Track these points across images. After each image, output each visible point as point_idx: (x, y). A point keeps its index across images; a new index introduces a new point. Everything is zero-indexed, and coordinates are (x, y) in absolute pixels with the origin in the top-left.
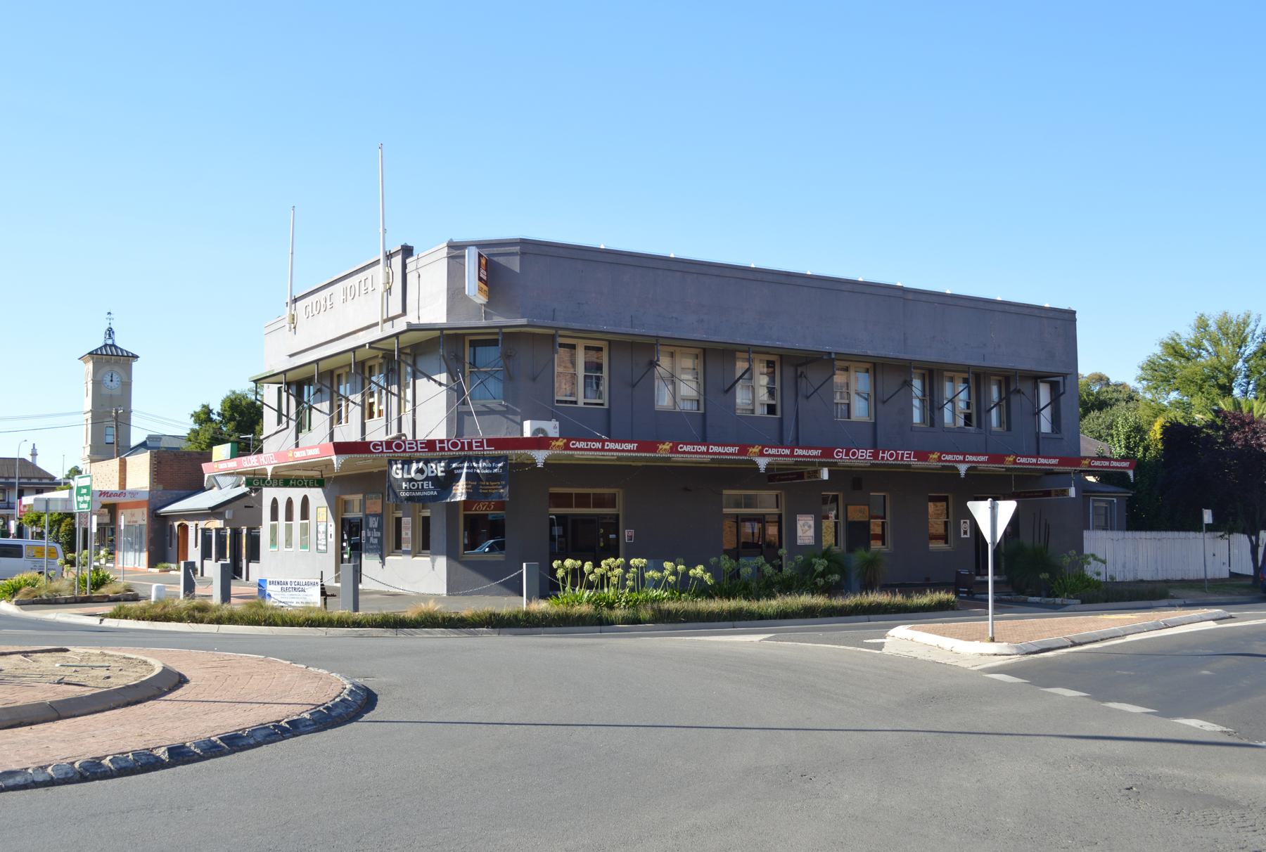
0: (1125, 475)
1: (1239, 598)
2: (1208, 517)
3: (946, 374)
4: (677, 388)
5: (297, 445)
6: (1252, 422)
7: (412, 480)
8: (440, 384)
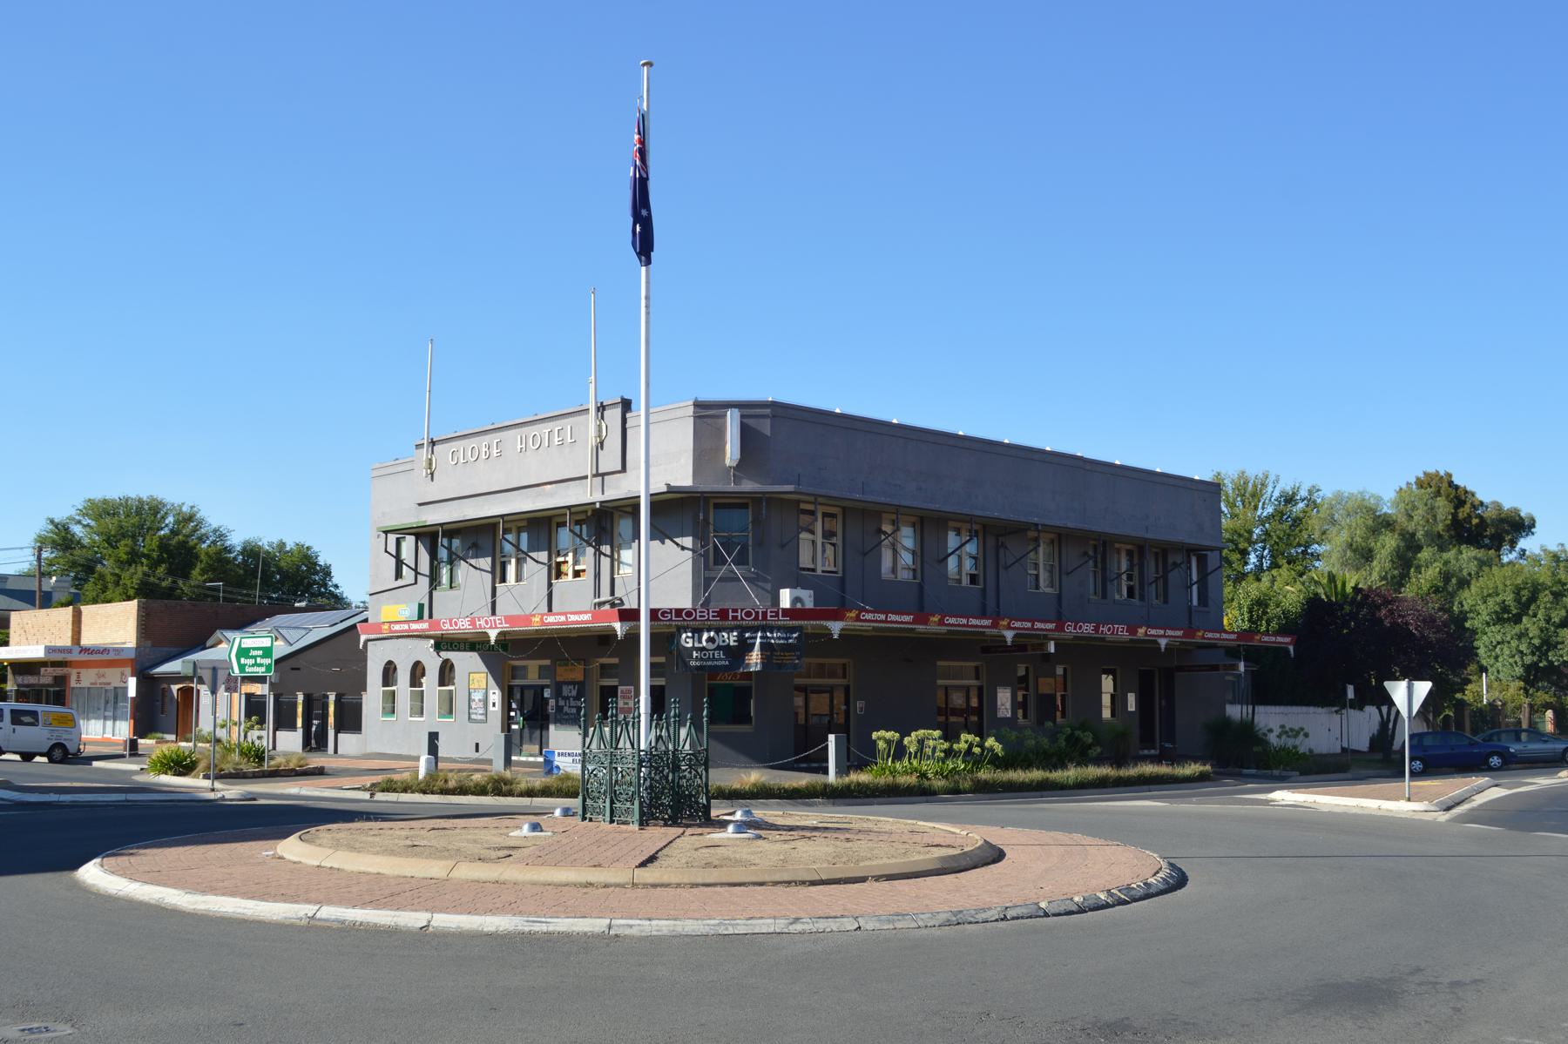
0: (1287, 651)
1: (1371, 772)
2: (1351, 693)
3: (951, 524)
4: (899, 554)
5: (550, 610)
6: (1366, 597)
7: (703, 649)
8: (683, 548)
